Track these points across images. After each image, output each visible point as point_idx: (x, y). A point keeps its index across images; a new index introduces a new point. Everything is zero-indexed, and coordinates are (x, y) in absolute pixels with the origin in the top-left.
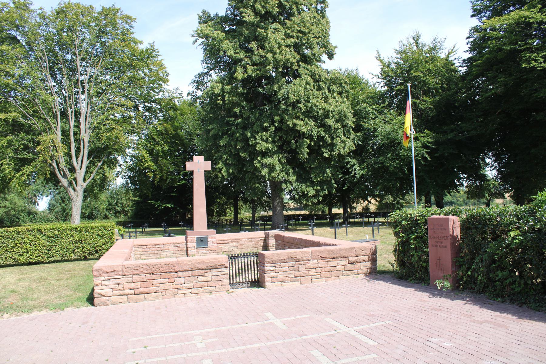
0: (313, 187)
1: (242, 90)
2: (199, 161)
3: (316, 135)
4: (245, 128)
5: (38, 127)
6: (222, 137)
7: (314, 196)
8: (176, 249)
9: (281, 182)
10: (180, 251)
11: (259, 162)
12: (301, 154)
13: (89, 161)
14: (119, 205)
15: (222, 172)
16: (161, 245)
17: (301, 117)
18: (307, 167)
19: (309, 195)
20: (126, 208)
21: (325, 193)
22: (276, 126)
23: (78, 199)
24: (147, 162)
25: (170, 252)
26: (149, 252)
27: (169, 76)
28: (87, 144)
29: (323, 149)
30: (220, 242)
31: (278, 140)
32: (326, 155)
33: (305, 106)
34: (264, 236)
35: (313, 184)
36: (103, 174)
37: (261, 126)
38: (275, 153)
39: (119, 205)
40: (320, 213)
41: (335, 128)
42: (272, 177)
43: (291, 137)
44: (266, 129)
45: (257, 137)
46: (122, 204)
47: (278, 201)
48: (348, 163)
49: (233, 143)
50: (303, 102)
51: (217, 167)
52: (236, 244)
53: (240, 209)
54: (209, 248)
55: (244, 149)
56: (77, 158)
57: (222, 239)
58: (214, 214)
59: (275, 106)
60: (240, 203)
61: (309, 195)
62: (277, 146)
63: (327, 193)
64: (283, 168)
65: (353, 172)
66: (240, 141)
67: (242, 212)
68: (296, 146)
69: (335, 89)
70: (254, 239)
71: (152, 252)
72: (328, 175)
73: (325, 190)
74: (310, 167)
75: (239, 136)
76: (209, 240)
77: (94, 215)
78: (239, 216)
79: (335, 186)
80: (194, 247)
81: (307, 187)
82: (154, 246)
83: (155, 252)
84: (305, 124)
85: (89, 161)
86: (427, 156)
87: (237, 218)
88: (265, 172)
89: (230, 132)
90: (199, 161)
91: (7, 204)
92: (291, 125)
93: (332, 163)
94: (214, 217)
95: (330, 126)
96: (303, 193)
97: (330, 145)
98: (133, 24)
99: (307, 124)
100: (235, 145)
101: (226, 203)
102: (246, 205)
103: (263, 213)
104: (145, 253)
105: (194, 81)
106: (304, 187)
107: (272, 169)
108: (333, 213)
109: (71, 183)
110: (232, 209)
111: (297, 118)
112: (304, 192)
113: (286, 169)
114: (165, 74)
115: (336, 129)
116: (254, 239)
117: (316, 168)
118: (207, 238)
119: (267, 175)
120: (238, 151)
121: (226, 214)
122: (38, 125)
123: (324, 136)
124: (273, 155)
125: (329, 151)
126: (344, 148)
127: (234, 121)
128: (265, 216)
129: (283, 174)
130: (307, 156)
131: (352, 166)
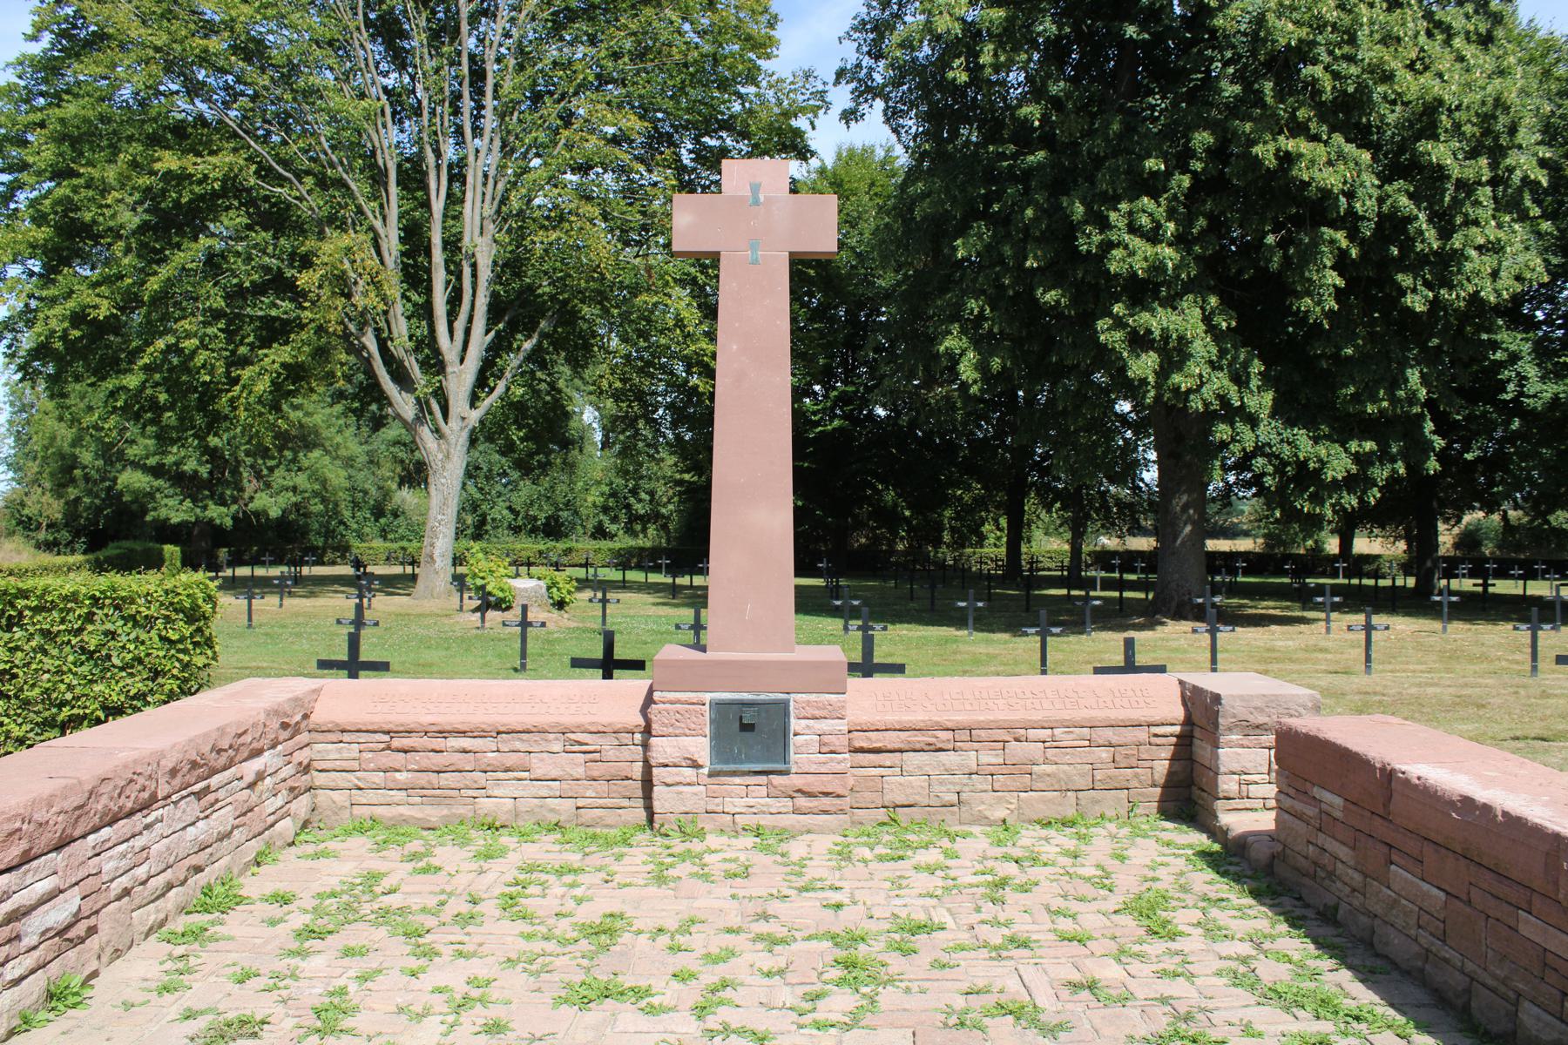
0: (1343, 445)
1: (1039, 451)
2: (755, 189)
3: (1372, 215)
4: (1060, 182)
5: (311, 209)
6: (962, 231)
7: (1349, 483)
8: (580, 771)
9: (1209, 418)
10: (602, 786)
11: (1119, 323)
12: (1309, 294)
13: (492, 333)
14: (643, 496)
15: (962, 367)
16: (482, 734)
17: (1313, 126)
19: (1329, 475)
20: (664, 506)
21: (1394, 471)
22: (1194, 174)
23: (449, 466)
24: (694, 342)
25: (542, 789)
26: (401, 777)
27: (779, 26)
28: (485, 274)
29: (1400, 277)
30: (877, 740)
31: (1203, 232)
32: (1417, 303)
33: (1336, 76)
34: (1179, 713)
36: (549, 384)
37: (1127, 172)
38: (1190, 286)
39: (643, 496)
41: (1461, 184)
42: (1176, 389)
43: (1263, 222)
44: (1153, 186)
45: (1113, 216)
46: (652, 493)
47: (1185, 498)
48: (1495, 346)
49: (1008, 251)
50: (1325, 58)
51: (942, 348)
52: (986, 758)
53: (1029, 526)
54: (795, 781)
55: (1053, 274)
56: (452, 315)
57: (891, 718)
58: (942, 537)
59: (1191, 96)
60: (1031, 504)
61: (1329, 475)
62: (1198, 258)
63: (1402, 471)
64: (1222, 353)
65: (1511, 387)
66: (1038, 240)
67: (1038, 534)
68: (1286, 257)
69: (1458, 23)
70: (1109, 734)
71: (424, 779)
72: (1414, 393)
73: (1393, 460)
74: (1337, 358)
75: (1036, 219)
76: (795, 724)
77: (563, 524)
78: (1024, 549)
79: (1439, 443)
80: (695, 765)
81: (1316, 443)
82: (438, 743)
83: (447, 779)
84: (1333, 156)
85: (492, 333)
87: (1019, 553)
88: (1144, 366)
89: (996, 207)
90: (755, 189)
91: (301, 480)
92: (1271, 162)
94: (944, 549)
95: (1439, 172)
96: (1302, 465)
97: (1423, 259)
99: (1341, 155)
100: (1015, 256)
101: (981, 503)
102: (1049, 511)
103: (1108, 542)
104: (378, 778)
105: (863, 23)
106: (1302, 438)
107: (1174, 353)
109: (422, 405)
110: (1003, 522)
111: (1298, 129)
112: (1307, 460)
113: (1235, 358)
114: (764, 19)
115: (1467, 188)
116: (1109, 734)
117: (1362, 359)
118: (782, 708)
119: (1151, 379)
120: (1028, 280)
121: (982, 538)
122: (308, 201)
123: (1411, 219)
124: (1180, 296)
126: (1495, 275)
127: (1014, 156)
128: (1114, 554)
129: (1220, 382)
130: (1331, 304)
131: (1514, 358)
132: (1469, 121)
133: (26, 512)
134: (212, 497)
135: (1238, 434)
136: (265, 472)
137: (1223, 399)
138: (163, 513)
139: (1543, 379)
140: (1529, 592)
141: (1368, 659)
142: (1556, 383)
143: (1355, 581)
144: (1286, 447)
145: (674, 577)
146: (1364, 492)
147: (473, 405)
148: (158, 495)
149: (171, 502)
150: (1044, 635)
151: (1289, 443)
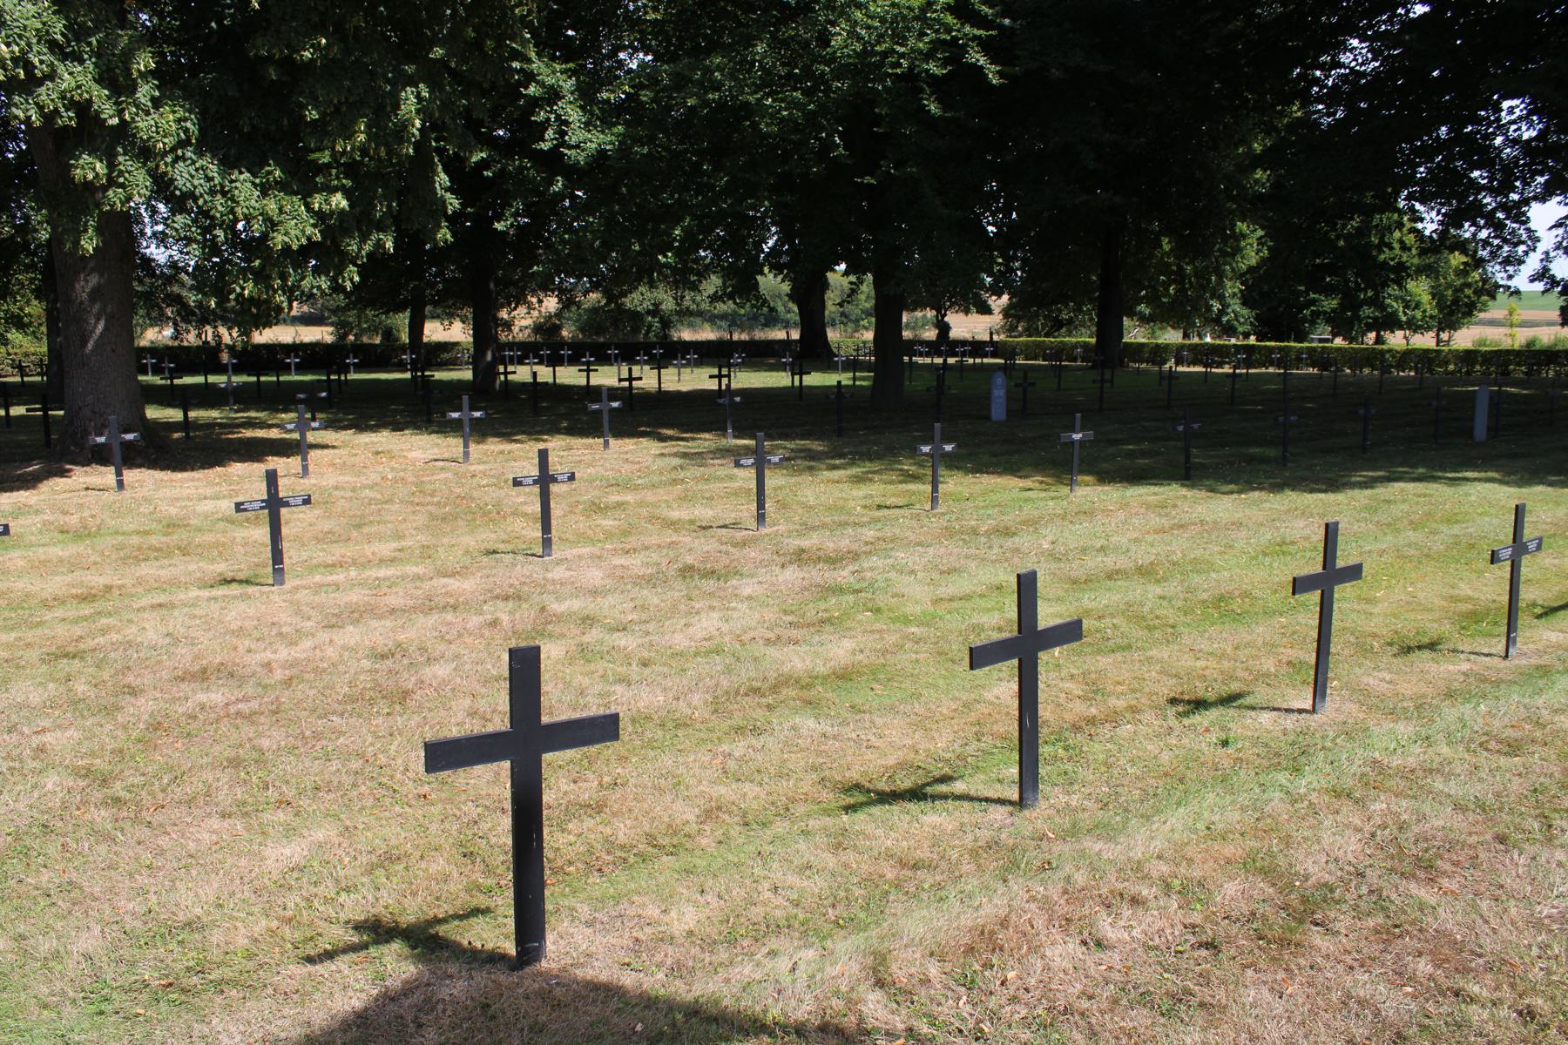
0: (306, 195)
18: (270, 59)
19: (279, 240)
21: (379, 244)
35: (302, 180)
40: (378, 341)
61: (279, 240)
63: (389, 245)
65: (550, 134)
79: (453, 203)
81: (264, 194)
86: (977, 57)
93: (438, 52)
108: (425, 340)
117: (328, 69)
129: (77, 78)
131: (554, 95)
135: (121, 173)
137: (83, 109)
139: (588, 125)
140: (665, 387)
141: (277, 556)
142: (603, 132)
144: (219, 198)
146: (340, 272)
151: (224, 194)
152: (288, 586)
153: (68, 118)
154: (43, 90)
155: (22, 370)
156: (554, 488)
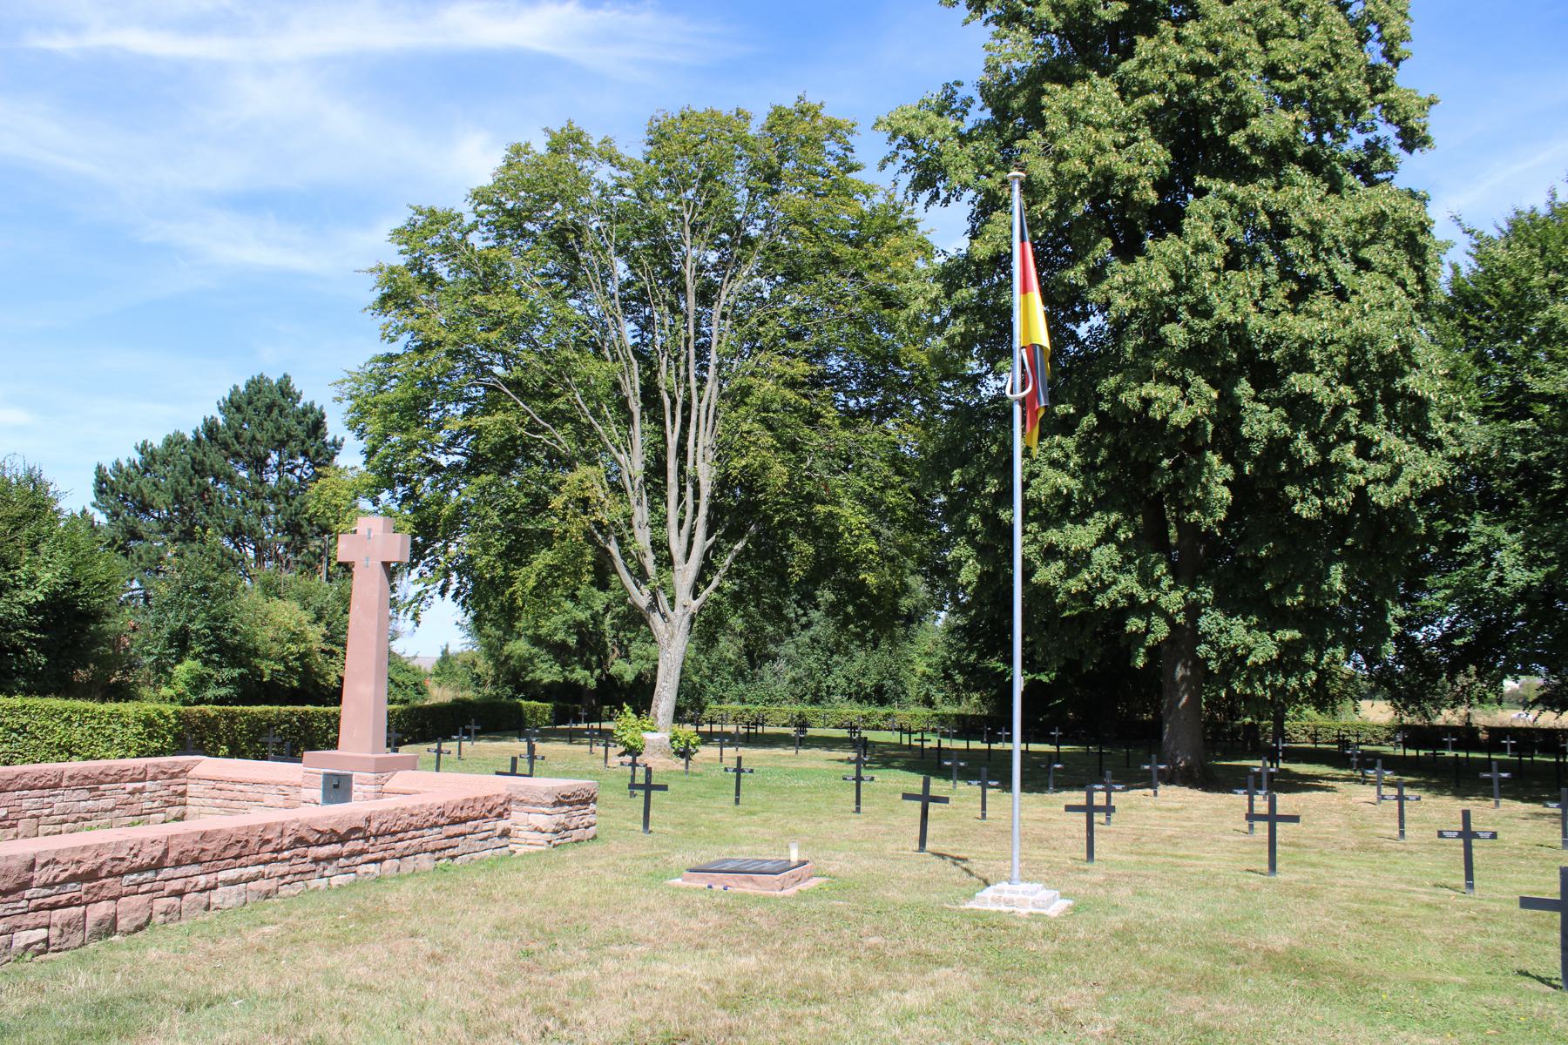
0: (1272, 632)
2: (370, 530)
7: (1272, 666)
8: (281, 804)
23: (674, 644)
32: (1306, 509)
76: (355, 787)
77: (886, 692)
82: (231, 787)
83: (234, 804)
97: (1311, 471)
98: (851, 140)
112: (1236, 647)
118: (348, 778)
125: (1316, 492)
129: (1128, 583)
132: (1339, 352)
133: (476, 671)
134: (580, 662)
136: (626, 642)
137: (1131, 597)
138: (538, 674)
143: (1462, 754)
145: (1520, 756)
146: (1303, 676)
147: (695, 597)
148: (536, 660)
149: (545, 666)
150: (984, 787)
152: (1477, 892)
153: (1123, 603)
154: (1109, 591)
155: (1314, 738)
156: (863, 783)
